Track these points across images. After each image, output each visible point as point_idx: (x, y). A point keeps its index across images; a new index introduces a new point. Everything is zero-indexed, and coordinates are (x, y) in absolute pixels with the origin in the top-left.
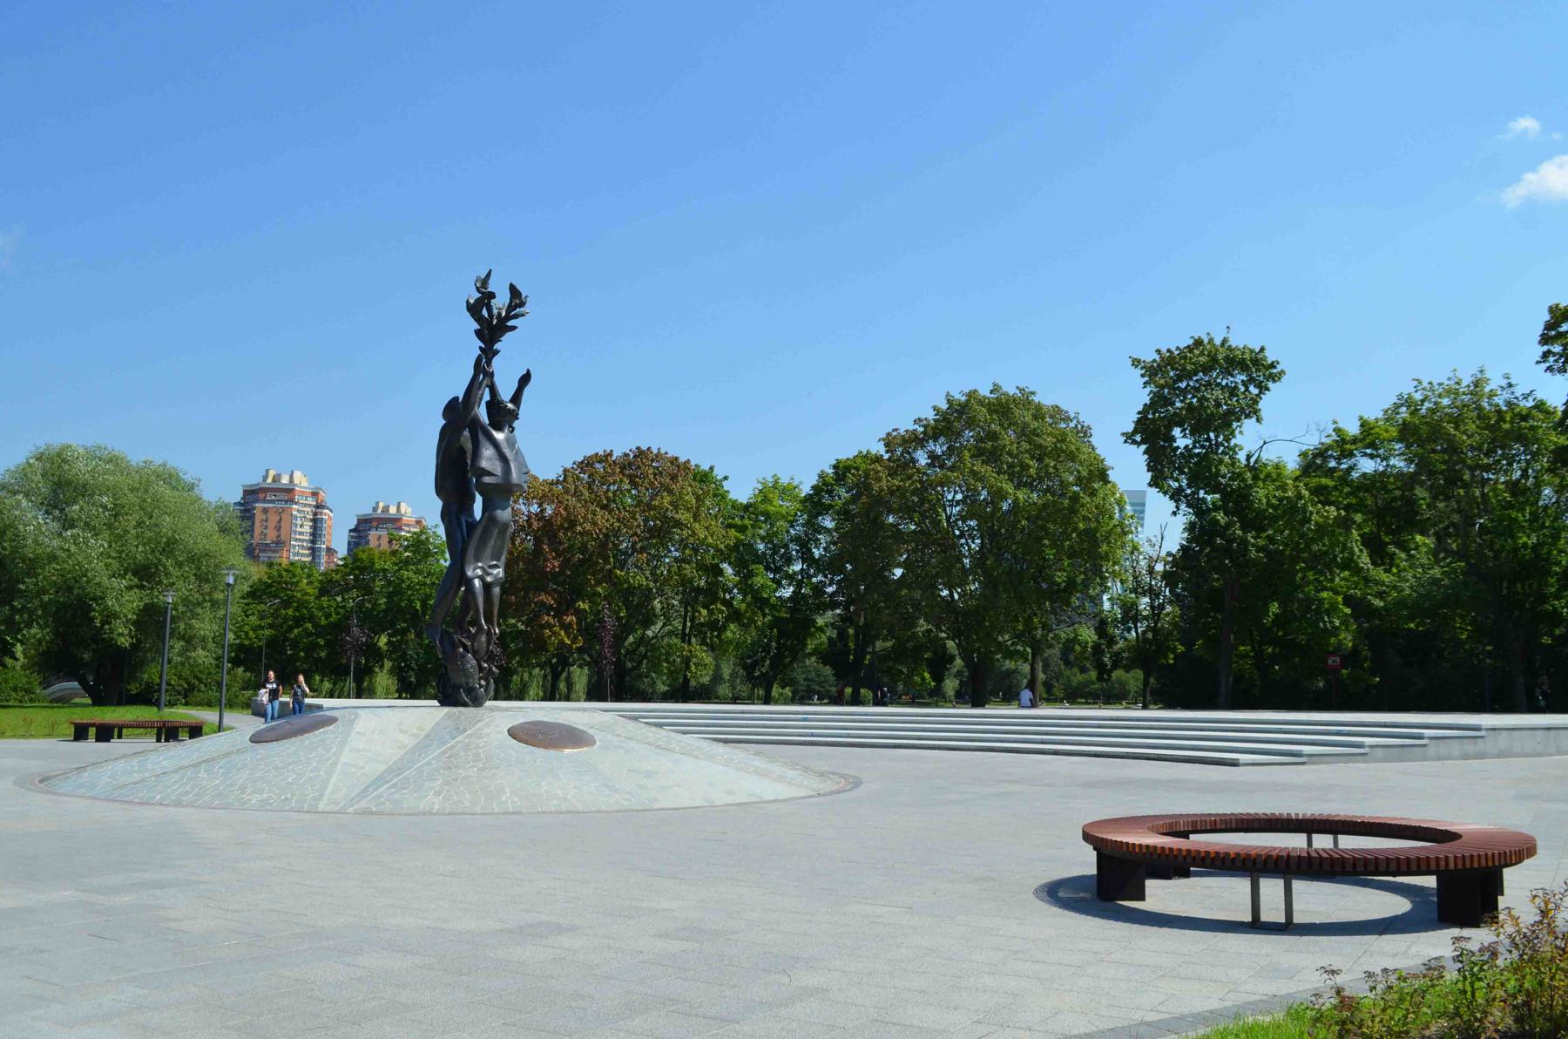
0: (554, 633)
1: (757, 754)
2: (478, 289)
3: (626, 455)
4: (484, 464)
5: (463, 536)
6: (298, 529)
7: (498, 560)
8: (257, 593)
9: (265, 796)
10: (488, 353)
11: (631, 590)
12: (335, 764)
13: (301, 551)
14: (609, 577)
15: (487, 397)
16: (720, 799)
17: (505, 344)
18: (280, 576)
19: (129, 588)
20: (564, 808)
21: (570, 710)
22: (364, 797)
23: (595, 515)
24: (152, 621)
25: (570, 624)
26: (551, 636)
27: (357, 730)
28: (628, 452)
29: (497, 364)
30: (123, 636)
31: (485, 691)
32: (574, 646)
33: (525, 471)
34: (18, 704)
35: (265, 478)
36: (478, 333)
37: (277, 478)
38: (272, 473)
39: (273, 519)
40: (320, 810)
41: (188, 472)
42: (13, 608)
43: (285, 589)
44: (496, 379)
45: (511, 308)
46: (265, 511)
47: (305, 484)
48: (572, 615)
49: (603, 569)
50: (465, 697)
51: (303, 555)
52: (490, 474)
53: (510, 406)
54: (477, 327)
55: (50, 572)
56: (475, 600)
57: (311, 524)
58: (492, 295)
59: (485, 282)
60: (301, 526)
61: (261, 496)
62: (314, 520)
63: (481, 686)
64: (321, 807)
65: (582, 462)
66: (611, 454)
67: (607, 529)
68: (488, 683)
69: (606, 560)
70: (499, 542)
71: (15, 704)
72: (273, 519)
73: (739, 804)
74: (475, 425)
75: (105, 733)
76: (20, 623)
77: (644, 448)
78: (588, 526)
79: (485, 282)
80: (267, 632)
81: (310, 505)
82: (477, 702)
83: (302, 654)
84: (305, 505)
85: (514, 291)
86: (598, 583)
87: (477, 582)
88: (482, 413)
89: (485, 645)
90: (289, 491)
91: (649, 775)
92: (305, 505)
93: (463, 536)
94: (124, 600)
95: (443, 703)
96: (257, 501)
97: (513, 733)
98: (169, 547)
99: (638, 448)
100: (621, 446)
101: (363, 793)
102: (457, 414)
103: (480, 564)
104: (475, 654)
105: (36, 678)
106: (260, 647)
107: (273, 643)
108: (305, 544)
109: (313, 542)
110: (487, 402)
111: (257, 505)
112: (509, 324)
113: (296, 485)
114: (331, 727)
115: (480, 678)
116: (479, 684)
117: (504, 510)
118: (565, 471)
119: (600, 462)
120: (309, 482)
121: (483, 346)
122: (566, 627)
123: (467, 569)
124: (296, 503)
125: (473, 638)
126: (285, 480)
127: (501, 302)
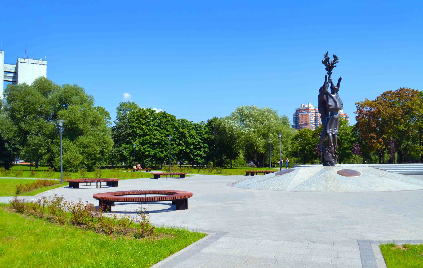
0: (376, 144)
1: (414, 177)
2: (325, 57)
3: (397, 91)
4: (330, 104)
5: (326, 122)
6: (311, 119)
7: (336, 128)
8: (296, 138)
9: (274, 187)
10: (330, 74)
11: (399, 131)
12: (291, 180)
13: (312, 125)
14: (392, 127)
15: (330, 85)
16: (393, 189)
17: (334, 71)
18: (302, 133)
19: (261, 139)
20: (346, 191)
21: (359, 166)
22: (297, 188)
23: (387, 109)
24: (267, 146)
25: (381, 141)
26: (375, 145)
27: (299, 172)
28: (397, 90)
29: (332, 76)
30: (262, 150)
31: (335, 162)
32: (382, 148)
33: (342, 104)
34: (241, 167)
35: (301, 106)
36: (327, 69)
37: (304, 106)
38: (303, 105)
39: (304, 117)
40: (286, 190)
41: (274, 109)
42: (236, 145)
43: (304, 136)
44: (332, 80)
45: (334, 61)
46: (302, 115)
47: (312, 107)
48: (381, 139)
49: (390, 125)
50: (329, 164)
51: (313, 126)
52: (331, 106)
53: (336, 87)
54: (326, 67)
55: (243, 138)
56: (330, 139)
57: (315, 117)
58: (329, 58)
59: (326, 55)
60: (312, 118)
61: (300, 111)
62: (315, 117)
63: (333, 161)
64: (287, 190)
65: (383, 94)
66: (391, 91)
67: (390, 113)
68: (335, 160)
69: (391, 122)
70: (336, 123)
71: (23, 162)
72: (304, 117)
73: (398, 191)
74: (327, 93)
75: (252, 174)
76: (237, 149)
77: (402, 88)
78: (384, 113)
79: (326, 55)
80: (300, 148)
81: (314, 113)
82: (332, 165)
83: (309, 153)
84: (313, 113)
85: (334, 56)
86: (389, 129)
87: (330, 134)
88: (329, 90)
89: (334, 150)
90: (308, 109)
91: (373, 183)
92: (313, 113)
93: (326, 122)
94: (261, 143)
95: (324, 165)
96: (299, 113)
97: (338, 173)
98: (269, 129)
99: (400, 88)
100: (395, 88)
101: (296, 187)
102: (323, 90)
103: (331, 130)
104: (331, 153)
105: (245, 162)
106: (298, 152)
107: (301, 150)
108: (313, 123)
109: (316, 122)
110: (331, 87)
111: (300, 114)
112: (335, 65)
113: (309, 107)
114: (293, 172)
115: (333, 159)
116: (333, 160)
117: (336, 115)
118: (378, 97)
119: (389, 93)
120: (313, 106)
121: (328, 72)
122: (380, 143)
123: (327, 131)
124: (310, 112)
125: (330, 148)
126: (306, 106)
127: (331, 60)
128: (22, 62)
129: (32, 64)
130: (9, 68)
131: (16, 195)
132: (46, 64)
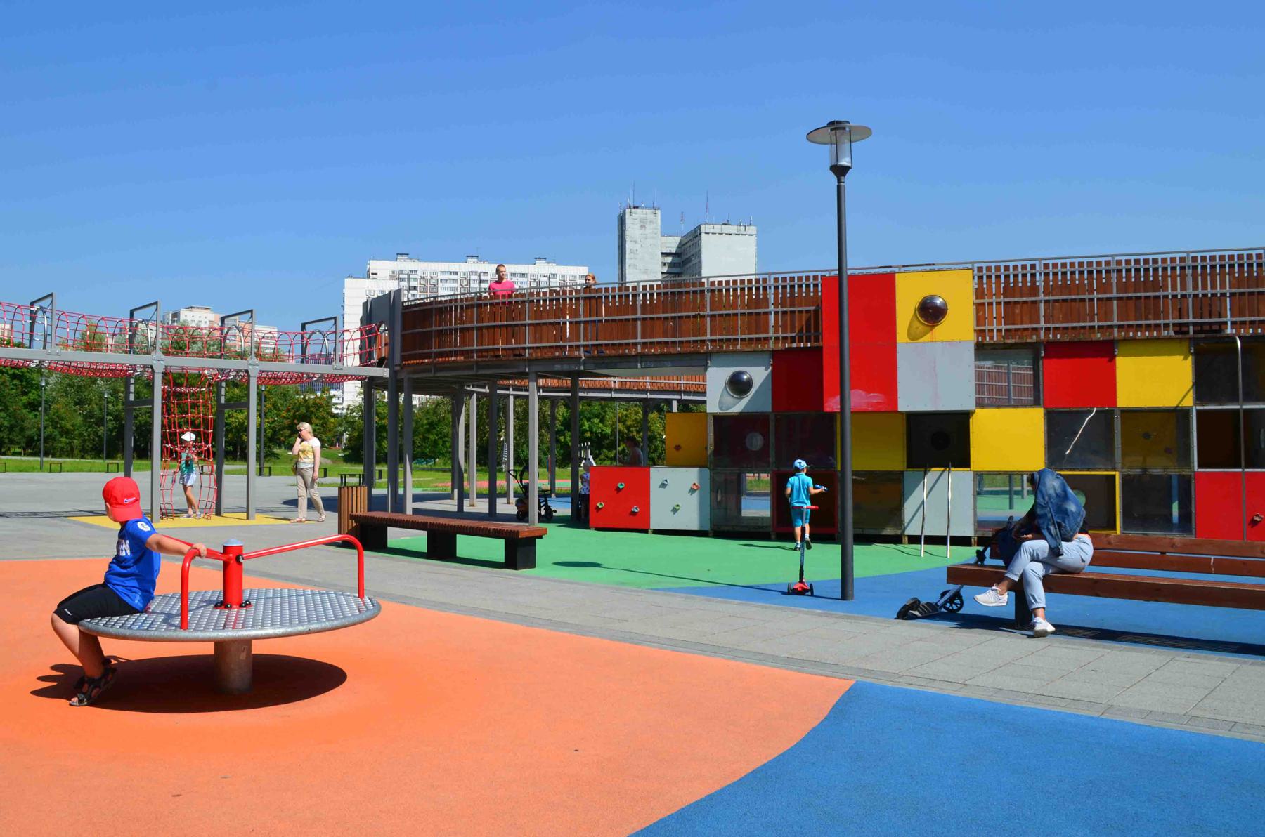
123: (359, 400)
128: (708, 233)
129: (728, 236)
130: (668, 245)
131: (1070, 516)
132: (755, 232)
